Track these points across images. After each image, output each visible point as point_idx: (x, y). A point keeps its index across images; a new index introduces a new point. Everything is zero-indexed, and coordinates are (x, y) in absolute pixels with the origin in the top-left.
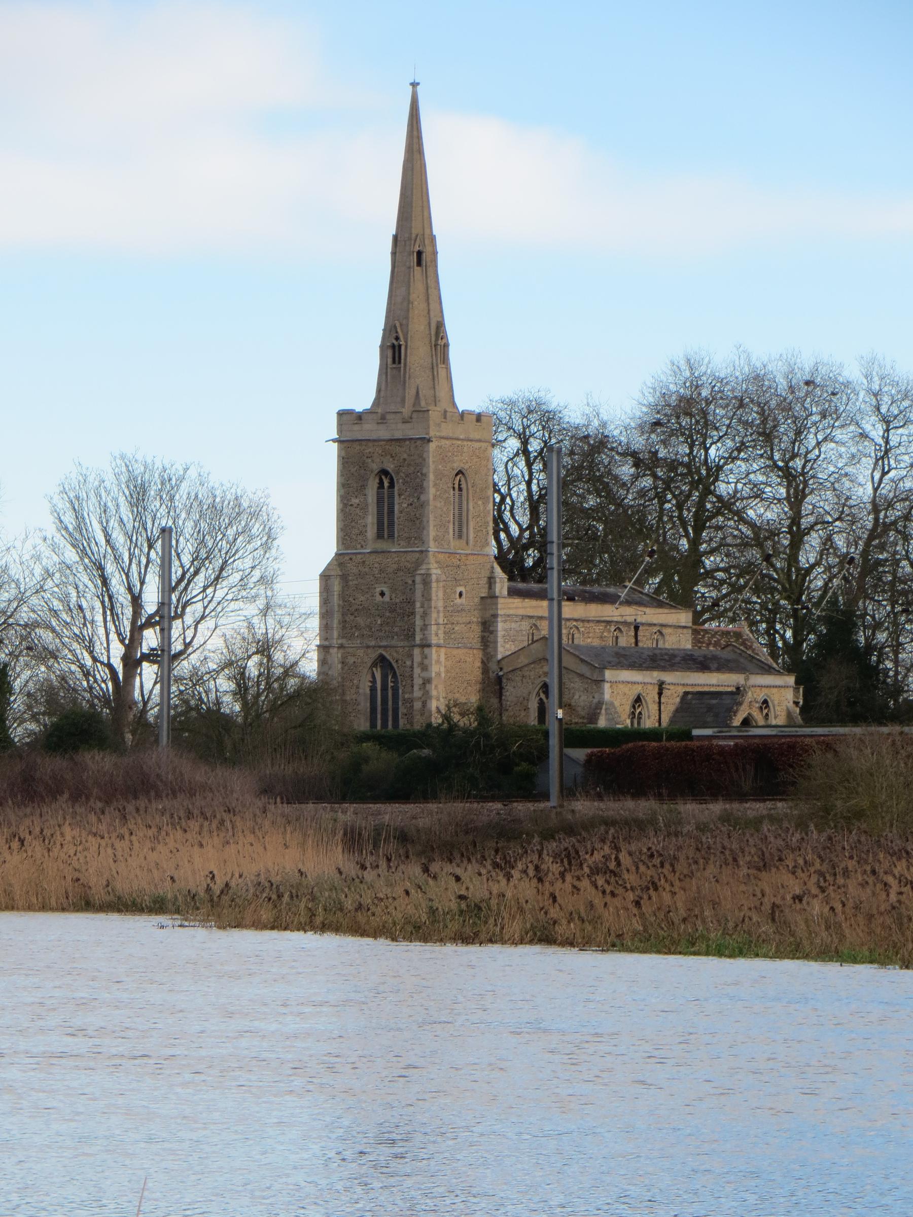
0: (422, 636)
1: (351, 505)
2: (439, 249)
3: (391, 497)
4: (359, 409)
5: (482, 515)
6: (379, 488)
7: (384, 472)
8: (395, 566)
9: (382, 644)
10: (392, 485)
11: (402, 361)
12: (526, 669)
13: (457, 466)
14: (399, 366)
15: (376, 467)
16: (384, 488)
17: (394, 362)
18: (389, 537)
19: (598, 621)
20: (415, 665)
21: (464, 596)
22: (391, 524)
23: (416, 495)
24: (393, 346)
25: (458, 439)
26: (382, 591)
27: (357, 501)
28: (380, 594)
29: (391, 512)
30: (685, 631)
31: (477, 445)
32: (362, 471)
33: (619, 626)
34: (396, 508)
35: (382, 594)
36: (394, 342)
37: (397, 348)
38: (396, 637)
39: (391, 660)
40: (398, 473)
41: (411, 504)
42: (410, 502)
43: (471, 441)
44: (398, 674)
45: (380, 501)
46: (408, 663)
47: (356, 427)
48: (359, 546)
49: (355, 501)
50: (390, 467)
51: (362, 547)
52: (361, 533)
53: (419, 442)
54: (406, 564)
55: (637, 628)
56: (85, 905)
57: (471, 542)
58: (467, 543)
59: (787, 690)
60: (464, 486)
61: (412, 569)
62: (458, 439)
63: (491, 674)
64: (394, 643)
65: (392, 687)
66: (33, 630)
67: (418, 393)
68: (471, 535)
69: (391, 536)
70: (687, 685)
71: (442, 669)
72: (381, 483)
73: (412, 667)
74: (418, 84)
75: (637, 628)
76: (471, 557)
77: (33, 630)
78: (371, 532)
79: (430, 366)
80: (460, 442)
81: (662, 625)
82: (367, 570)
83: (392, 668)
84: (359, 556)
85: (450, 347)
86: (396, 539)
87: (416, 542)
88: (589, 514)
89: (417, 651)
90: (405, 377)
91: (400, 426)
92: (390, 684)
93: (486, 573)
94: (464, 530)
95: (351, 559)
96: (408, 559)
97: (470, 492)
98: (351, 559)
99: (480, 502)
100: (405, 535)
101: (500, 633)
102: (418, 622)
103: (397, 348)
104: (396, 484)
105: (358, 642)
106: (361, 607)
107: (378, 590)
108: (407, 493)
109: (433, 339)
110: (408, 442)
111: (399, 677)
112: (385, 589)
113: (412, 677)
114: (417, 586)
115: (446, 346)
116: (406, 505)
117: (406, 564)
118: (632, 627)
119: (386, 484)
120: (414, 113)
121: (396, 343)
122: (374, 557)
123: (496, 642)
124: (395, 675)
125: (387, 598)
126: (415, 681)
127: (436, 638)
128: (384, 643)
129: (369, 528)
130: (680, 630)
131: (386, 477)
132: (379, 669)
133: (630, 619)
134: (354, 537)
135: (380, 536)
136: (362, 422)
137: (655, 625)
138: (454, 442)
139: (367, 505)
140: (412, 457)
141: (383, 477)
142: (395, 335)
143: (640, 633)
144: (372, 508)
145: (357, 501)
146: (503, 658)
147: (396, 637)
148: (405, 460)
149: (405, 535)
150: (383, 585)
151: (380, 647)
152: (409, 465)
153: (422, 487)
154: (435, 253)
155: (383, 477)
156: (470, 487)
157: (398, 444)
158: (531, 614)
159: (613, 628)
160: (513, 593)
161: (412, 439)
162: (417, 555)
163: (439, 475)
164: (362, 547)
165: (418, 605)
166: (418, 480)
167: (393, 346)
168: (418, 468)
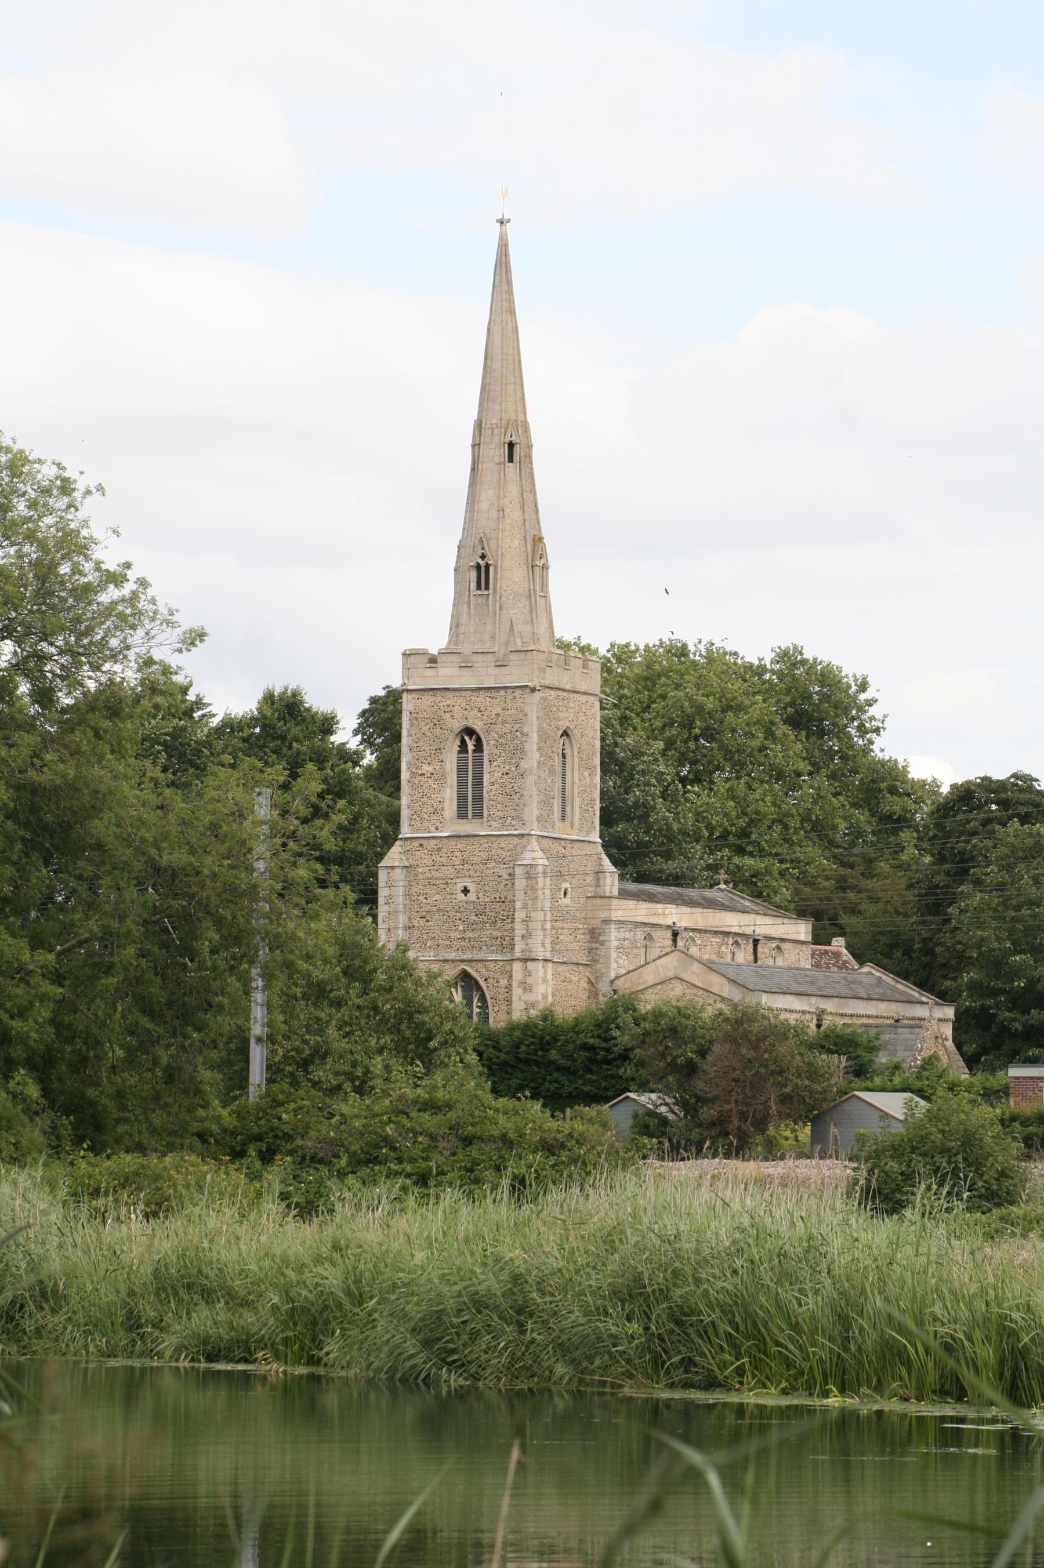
0: (524, 946)
1: (422, 774)
2: (534, 440)
3: (479, 764)
4: (434, 651)
5: (588, 789)
6: (459, 752)
7: (470, 732)
8: (484, 855)
9: (465, 957)
10: (479, 747)
11: (491, 586)
12: (651, 991)
13: (563, 725)
14: (486, 592)
15: (457, 725)
16: (467, 752)
17: (479, 587)
18: (474, 815)
19: (716, 932)
20: (515, 984)
21: (569, 895)
22: (479, 799)
23: (513, 761)
24: (478, 567)
25: (564, 690)
26: (465, 888)
27: (430, 769)
28: (468, 891)
29: (478, 783)
30: (804, 947)
31: (583, 698)
32: (438, 731)
33: (737, 938)
34: (486, 778)
35: (466, 891)
36: (480, 561)
37: (483, 569)
38: (484, 948)
39: (478, 979)
40: (488, 732)
41: (507, 774)
42: (505, 770)
43: (578, 692)
44: (488, 997)
45: (462, 769)
46: (503, 982)
47: (429, 672)
48: (433, 829)
49: (427, 769)
50: (478, 726)
51: (437, 829)
52: (435, 812)
53: (518, 692)
54: (499, 852)
55: (756, 942)
56: (133, 1290)
57: (577, 825)
58: (572, 827)
59: (946, 1024)
60: (568, 752)
61: (508, 859)
62: (564, 690)
63: (601, 998)
64: (481, 956)
65: (478, 1013)
66: (118, 933)
67: (512, 628)
68: (577, 816)
69: (478, 814)
70: (846, 1015)
71: (550, 991)
72: (463, 745)
73: (509, 987)
74: (509, 221)
75: (756, 942)
76: (577, 845)
77: (118, 933)
78: (450, 807)
79: (527, 592)
80: (565, 694)
81: (783, 940)
82: (443, 860)
83: (479, 988)
84: (433, 842)
85: (550, 570)
86: (485, 819)
87: (514, 823)
88: (966, 806)
89: (517, 966)
90: (494, 606)
91: (493, 671)
92: (476, 1010)
93: (591, 867)
94: (568, 809)
95: (421, 845)
96: (503, 845)
97: (576, 759)
98: (421, 845)
99: (586, 774)
100: (498, 814)
101: (614, 944)
102: (519, 929)
103: (483, 569)
104: (485, 746)
105: (432, 954)
106: (435, 909)
107: (460, 887)
108: (501, 760)
109: (530, 559)
110: (502, 692)
111: (489, 1001)
112: (471, 887)
113: (509, 1002)
114: (517, 882)
115: (545, 568)
116: (500, 774)
117: (499, 852)
118: (751, 941)
119: (471, 745)
120: (504, 260)
121: (482, 563)
122: (454, 843)
123: (608, 957)
124: (483, 998)
125: (472, 897)
126: (514, 1005)
127: (542, 949)
128: (468, 956)
129: (446, 805)
130: (799, 946)
131: (471, 739)
132: (459, 990)
133: (748, 931)
134: (426, 816)
135: (462, 814)
136: (439, 665)
137: (774, 938)
138: (560, 693)
139: (444, 775)
140: (508, 713)
141: (467, 738)
142: (480, 552)
143: (760, 949)
144: (452, 779)
145: (430, 769)
146: (617, 978)
147: (484, 948)
148: (498, 715)
149: (498, 814)
150: (466, 879)
151: (463, 961)
152: (504, 722)
153: (522, 751)
154: (529, 446)
155: (467, 738)
156: (576, 753)
157: (488, 694)
158: (646, 921)
159: (731, 941)
160: (624, 894)
161: (506, 687)
162: (516, 840)
163: (543, 737)
164: (437, 829)
165: (518, 905)
166: (516, 742)
167: (478, 567)
168: (517, 726)
